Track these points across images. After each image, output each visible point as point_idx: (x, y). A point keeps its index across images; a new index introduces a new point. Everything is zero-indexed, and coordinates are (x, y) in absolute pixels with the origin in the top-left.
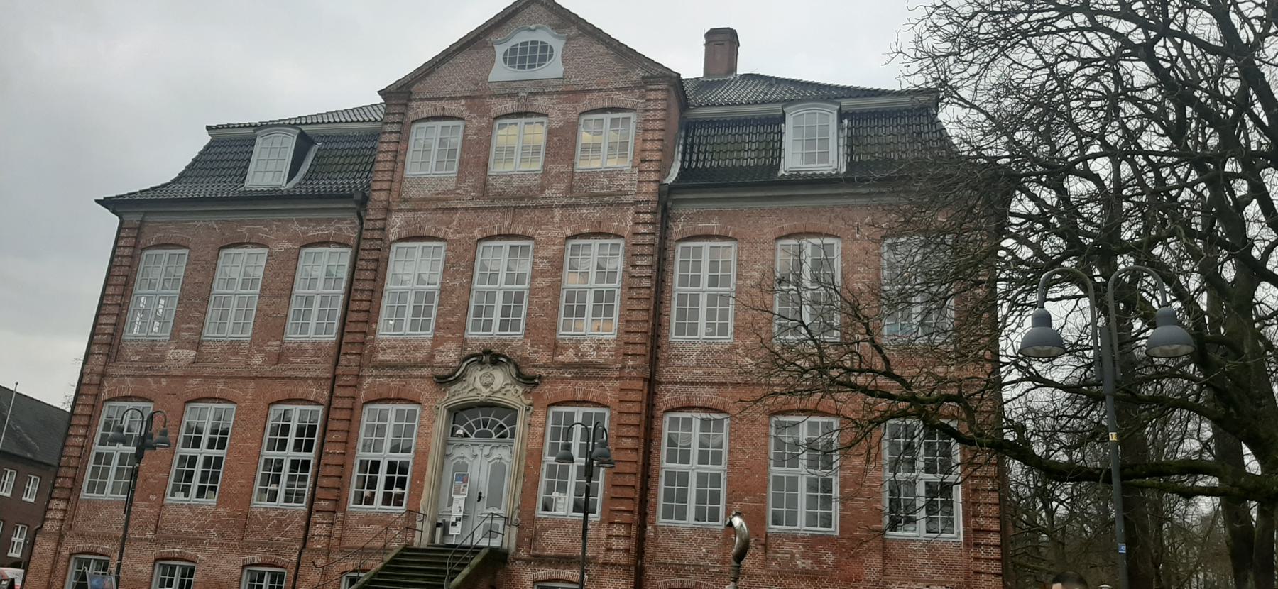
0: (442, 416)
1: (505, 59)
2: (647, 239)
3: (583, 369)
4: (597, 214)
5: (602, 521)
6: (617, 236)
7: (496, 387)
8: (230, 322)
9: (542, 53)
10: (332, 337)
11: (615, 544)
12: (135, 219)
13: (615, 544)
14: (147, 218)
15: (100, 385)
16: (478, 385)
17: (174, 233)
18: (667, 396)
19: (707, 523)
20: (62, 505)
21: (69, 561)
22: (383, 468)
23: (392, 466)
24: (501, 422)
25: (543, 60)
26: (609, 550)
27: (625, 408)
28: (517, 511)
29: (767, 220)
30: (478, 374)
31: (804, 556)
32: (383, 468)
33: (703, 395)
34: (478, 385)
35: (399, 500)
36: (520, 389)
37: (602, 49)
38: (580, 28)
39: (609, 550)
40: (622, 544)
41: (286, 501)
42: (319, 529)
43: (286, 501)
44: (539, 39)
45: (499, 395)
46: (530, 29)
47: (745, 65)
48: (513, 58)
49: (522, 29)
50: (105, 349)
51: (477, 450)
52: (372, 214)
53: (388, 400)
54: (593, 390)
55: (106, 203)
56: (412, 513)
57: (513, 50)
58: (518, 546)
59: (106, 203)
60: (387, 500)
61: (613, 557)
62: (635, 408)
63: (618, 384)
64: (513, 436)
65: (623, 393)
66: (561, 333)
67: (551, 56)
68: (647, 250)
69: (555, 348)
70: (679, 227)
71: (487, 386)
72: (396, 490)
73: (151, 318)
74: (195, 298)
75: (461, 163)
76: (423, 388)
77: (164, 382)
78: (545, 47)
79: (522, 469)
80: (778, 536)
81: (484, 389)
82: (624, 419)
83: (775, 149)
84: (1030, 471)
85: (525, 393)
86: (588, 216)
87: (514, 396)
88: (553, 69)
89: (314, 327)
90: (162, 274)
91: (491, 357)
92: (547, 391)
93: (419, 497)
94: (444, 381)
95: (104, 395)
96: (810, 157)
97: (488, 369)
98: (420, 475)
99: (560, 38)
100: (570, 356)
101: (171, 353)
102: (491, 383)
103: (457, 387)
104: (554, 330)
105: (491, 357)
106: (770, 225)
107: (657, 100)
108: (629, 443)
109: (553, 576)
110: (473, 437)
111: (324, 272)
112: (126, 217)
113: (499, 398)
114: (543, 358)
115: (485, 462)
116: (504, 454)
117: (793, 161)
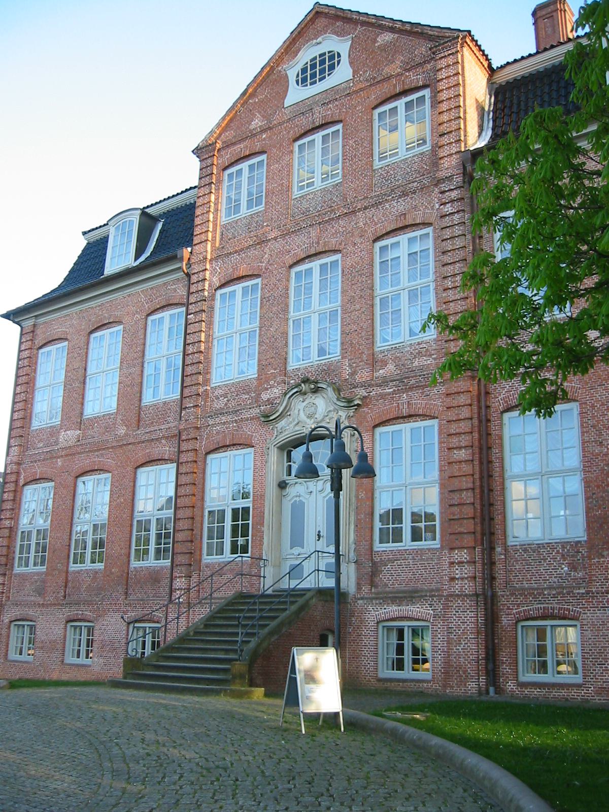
0: (274, 456)
1: (297, 82)
2: (459, 243)
4: (400, 206)
5: (442, 548)
7: (319, 416)
8: (102, 399)
10: (177, 395)
11: (457, 572)
12: (28, 324)
13: (457, 572)
14: (41, 320)
15: (18, 473)
16: (303, 416)
17: (57, 330)
21: (9, 627)
23: (235, 512)
26: (453, 579)
28: (353, 546)
34: (303, 416)
35: (245, 549)
37: (553, 525)
39: (453, 579)
40: (467, 570)
42: (179, 583)
54: (418, 401)
55: (7, 316)
57: (304, 70)
58: (359, 586)
59: (7, 316)
60: (234, 550)
61: (457, 587)
62: (465, 413)
65: (449, 400)
67: (339, 62)
68: (457, 231)
69: (374, 362)
71: (310, 416)
72: (241, 541)
73: (47, 406)
74: (76, 384)
79: (354, 500)
81: (308, 421)
82: (453, 428)
84: (594, 361)
89: (161, 389)
90: (52, 365)
93: (261, 544)
94: (267, 419)
95: (22, 482)
97: (310, 398)
98: (260, 522)
103: (282, 423)
105: (310, 384)
108: (463, 454)
109: (396, 614)
112: (24, 324)
114: (363, 375)
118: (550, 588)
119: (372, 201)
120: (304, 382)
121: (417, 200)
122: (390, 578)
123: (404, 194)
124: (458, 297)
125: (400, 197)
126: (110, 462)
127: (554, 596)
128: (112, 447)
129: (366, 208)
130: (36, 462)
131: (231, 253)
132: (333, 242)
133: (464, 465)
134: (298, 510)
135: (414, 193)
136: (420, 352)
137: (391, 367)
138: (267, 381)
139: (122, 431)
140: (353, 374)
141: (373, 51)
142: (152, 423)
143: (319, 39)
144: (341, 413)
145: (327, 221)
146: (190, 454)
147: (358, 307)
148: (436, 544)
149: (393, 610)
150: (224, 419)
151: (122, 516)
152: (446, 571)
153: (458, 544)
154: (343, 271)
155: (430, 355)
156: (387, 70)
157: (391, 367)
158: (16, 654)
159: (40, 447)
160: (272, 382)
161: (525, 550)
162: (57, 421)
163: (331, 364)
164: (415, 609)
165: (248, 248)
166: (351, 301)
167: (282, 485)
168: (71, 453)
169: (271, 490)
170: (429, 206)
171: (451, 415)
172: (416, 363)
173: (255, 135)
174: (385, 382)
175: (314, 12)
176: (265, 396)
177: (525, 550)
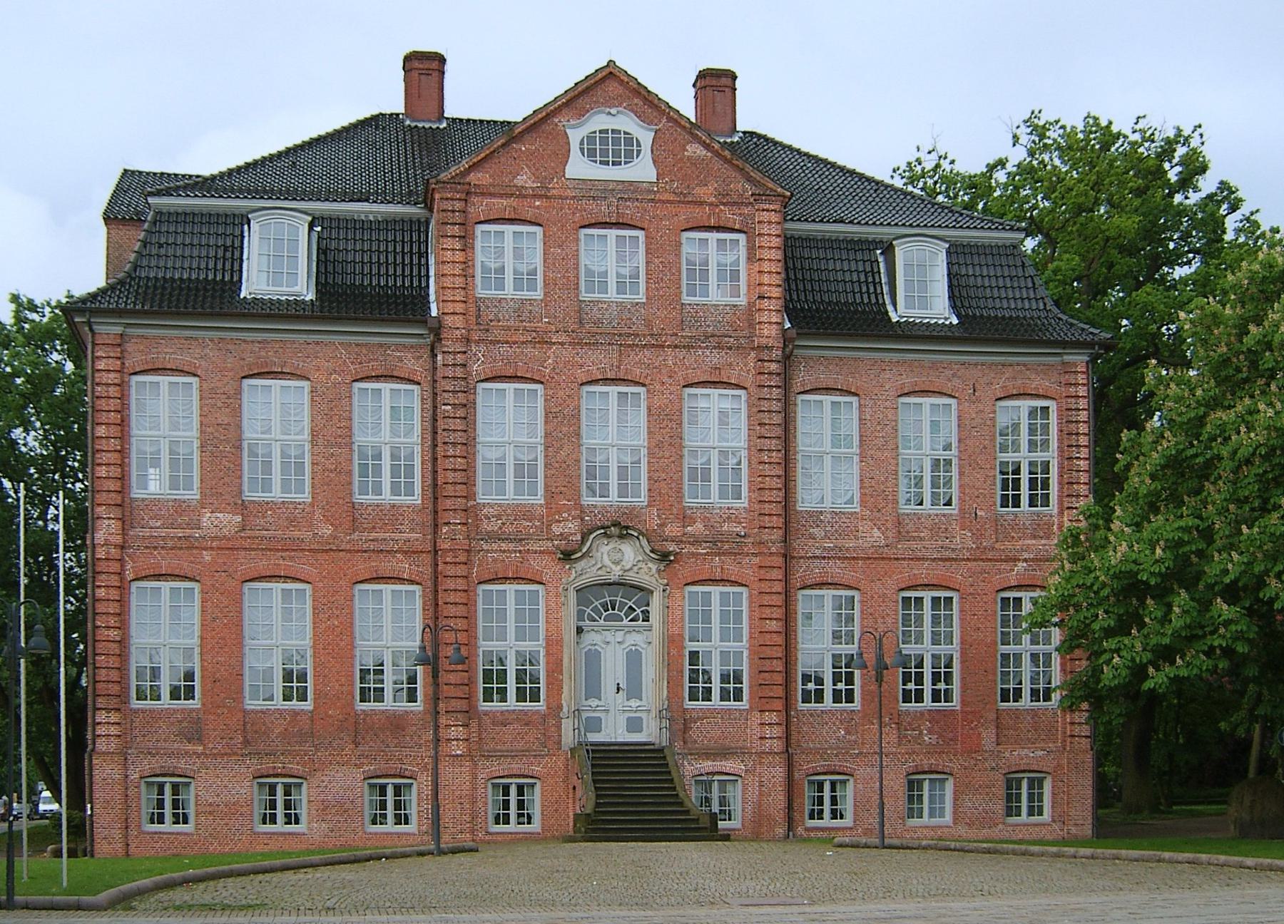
0: (572, 595)
1: (582, 150)
3: (717, 543)
4: (715, 358)
6: (738, 386)
9: (623, 149)
16: (607, 561)
18: (800, 571)
19: (844, 704)
20: (114, 717)
22: (1025, 500)
24: (630, 604)
25: (630, 156)
27: (765, 587)
29: (887, 375)
30: (605, 549)
31: (930, 732)
32: (1025, 500)
33: (835, 569)
34: (607, 561)
36: (654, 567)
38: (670, 119)
41: (1030, 506)
43: (1030, 506)
44: (623, 129)
45: (631, 573)
46: (609, 113)
47: (455, 107)
48: (591, 150)
49: (600, 112)
50: (116, 512)
51: (608, 636)
52: (449, 345)
53: (505, 579)
54: (732, 568)
56: (555, 709)
57: (591, 138)
63: (756, 560)
64: (646, 619)
66: (688, 501)
70: (802, 377)
71: (617, 563)
75: (546, 285)
76: (546, 566)
77: (207, 556)
78: (629, 140)
80: (908, 713)
81: (613, 567)
83: (233, 255)
85: (659, 571)
86: (598, 361)
87: (648, 574)
88: (642, 170)
91: (619, 527)
92: (685, 570)
95: (129, 575)
96: (275, 277)
99: (650, 130)
100: (698, 528)
101: (207, 518)
102: (622, 559)
103: (582, 564)
104: (680, 498)
105: (619, 527)
106: (892, 380)
107: (770, 222)
110: (602, 622)
111: (389, 421)
113: (632, 577)
115: (619, 649)
116: (636, 639)
117: (257, 281)
118: (831, 748)
119: (685, 342)
120: (614, 525)
121: (731, 358)
122: (701, 734)
123: (719, 347)
124: (772, 473)
125: (715, 348)
126: (306, 569)
127: (836, 755)
128: (309, 550)
129: (676, 347)
130: (155, 548)
131: (499, 342)
132: (637, 373)
133: (775, 635)
134: (593, 660)
135: (730, 348)
136: (729, 518)
137: (699, 526)
138: (560, 513)
139: (327, 530)
140: (662, 525)
141: (681, 159)
142: (374, 528)
143: (613, 111)
144: (650, 565)
145: (629, 346)
146: (460, 581)
147: (667, 454)
148: (744, 704)
149: (708, 765)
150: (504, 546)
151: (338, 645)
152: (757, 732)
153: (768, 707)
154: (649, 409)
155: (740, 523)
156: (700, 192)
157: (699, 526)
158: (378, 819)
159: (154, 528)
160: (565, 515)
161: (811, 715)
162: (194, 494)
163: (634, 508)
164: (729, 765)
165: (523, 343)
166: (659, 445)
167: (580, 631)
168: (228, 546)
169: (569, 635)
170: (744, 368)
171: (765, 587)
172: (725, 528)
173: (525, 197)
174: (696, 542)
175: (607, 70)
176: (557, 529)
177: (811, 715)
